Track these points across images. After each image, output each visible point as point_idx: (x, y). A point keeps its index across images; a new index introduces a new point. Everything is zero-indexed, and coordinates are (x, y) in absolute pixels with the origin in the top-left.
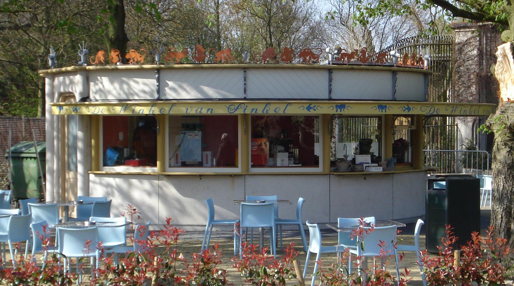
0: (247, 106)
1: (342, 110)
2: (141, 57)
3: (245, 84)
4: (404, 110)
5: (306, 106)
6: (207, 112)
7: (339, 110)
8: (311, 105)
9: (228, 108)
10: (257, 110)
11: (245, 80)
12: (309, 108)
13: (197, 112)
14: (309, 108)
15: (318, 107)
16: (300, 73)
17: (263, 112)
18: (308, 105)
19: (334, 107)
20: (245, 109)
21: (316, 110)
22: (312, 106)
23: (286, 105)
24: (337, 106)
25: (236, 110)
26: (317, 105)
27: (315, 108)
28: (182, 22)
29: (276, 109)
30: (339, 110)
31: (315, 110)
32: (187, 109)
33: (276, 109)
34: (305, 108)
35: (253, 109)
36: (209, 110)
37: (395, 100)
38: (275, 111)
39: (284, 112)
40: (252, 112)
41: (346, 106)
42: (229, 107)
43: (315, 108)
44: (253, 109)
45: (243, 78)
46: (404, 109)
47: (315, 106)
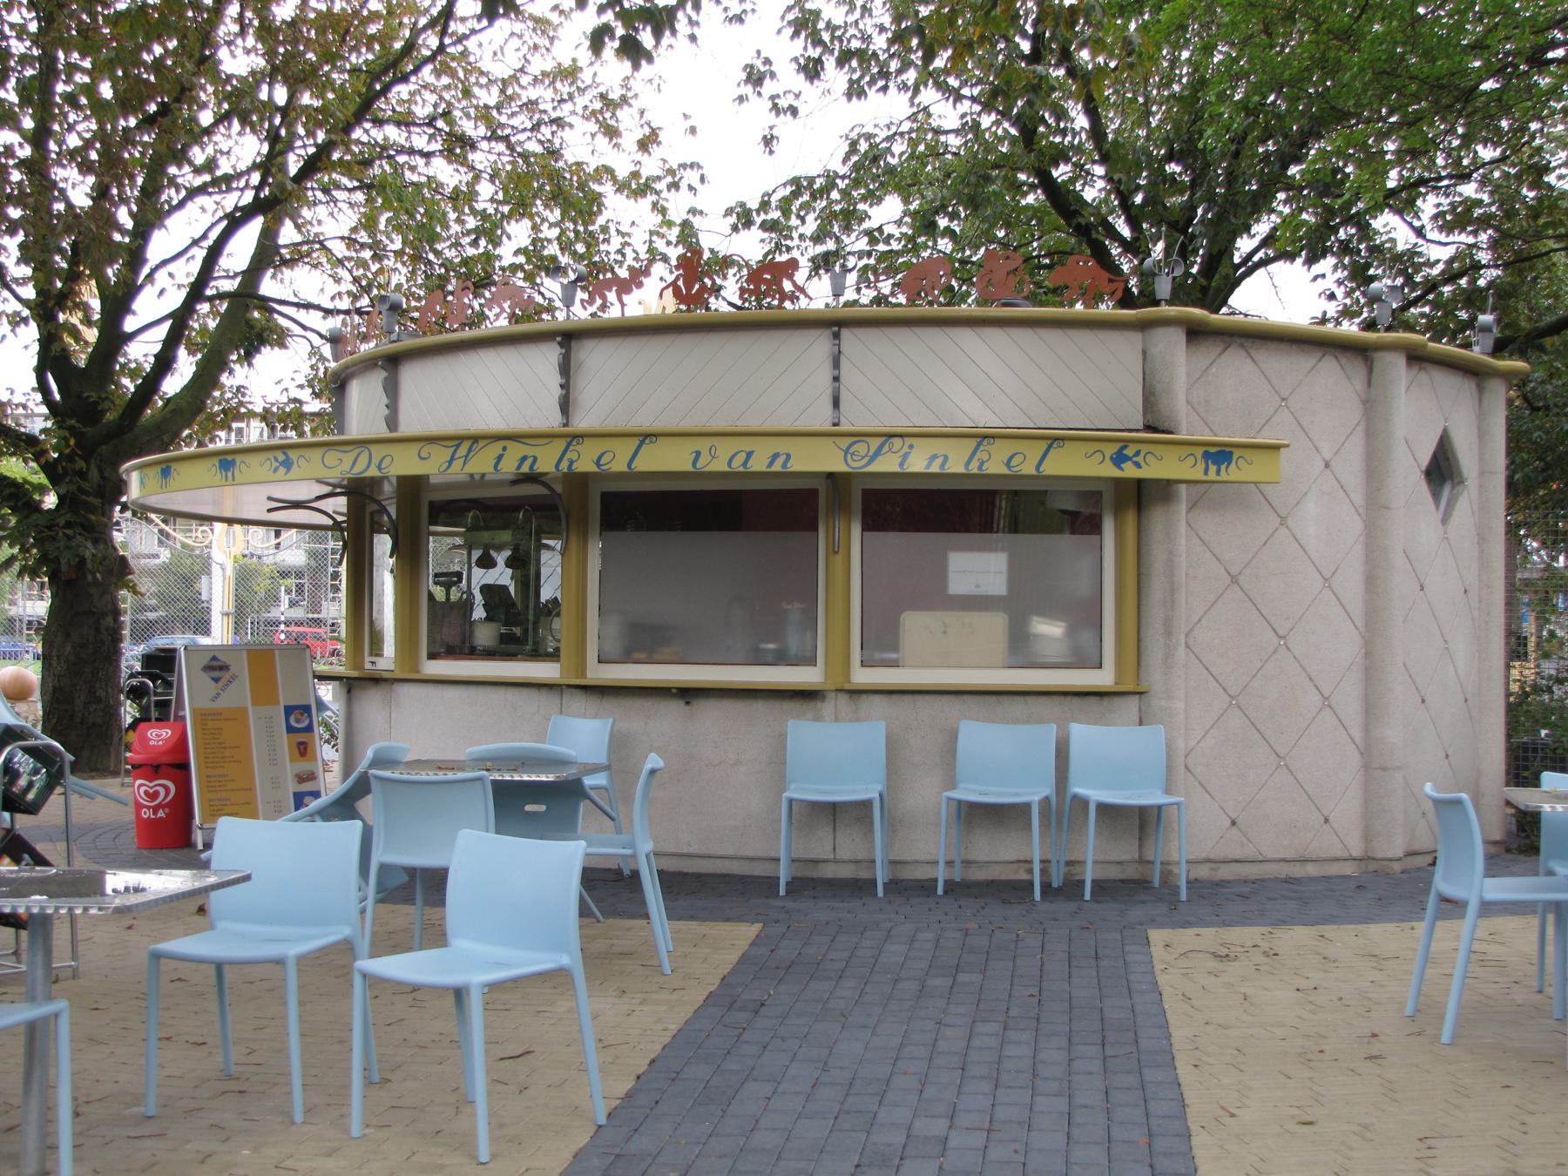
0: (504, 449)
1: (1223, 467)
2: (1111, 281)
3: (836, 379)
4: (276, 470)
5: (1111, 449)
6: (928, 466)
7: (1213, 468)
8: (1125, 447)
9: (846, 452)
10: (535, 459)
11: (836, 364)
12: (1119, 459)
13: (698, 466)
14: (1119, 459)
15: (1149, 456)
16: (509, 355)
17: (557, 466)
18: (1115, 447)
19: (1199, 457)
20: (906, 456)
21: (1142, 464)
22: (1129, 452)
23: (1043, 445)
24: (1206, 455)
25: (873, 459)
26: (1144, 448)
27: (1139, 459)
28: (814, 197)
29: (734, 456)
30: (1213, 468)
31: (1138, 465)
32: (698, 454)
33: (734, 456)
34: (1107, 458)
35: (524, 458)
36: (934, 457)
37: (1155, 430)
38: (1008, 464)
39: (1038, 468)
40: (770, 465)
41: (1235, 457)
42: (848, 448)
43: (1139, 459)
44: (524, 458)
45: (831, 359)
46: (275, 464)
47: (1138, 453)
